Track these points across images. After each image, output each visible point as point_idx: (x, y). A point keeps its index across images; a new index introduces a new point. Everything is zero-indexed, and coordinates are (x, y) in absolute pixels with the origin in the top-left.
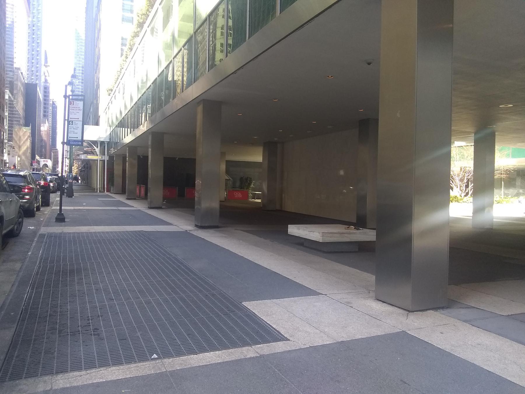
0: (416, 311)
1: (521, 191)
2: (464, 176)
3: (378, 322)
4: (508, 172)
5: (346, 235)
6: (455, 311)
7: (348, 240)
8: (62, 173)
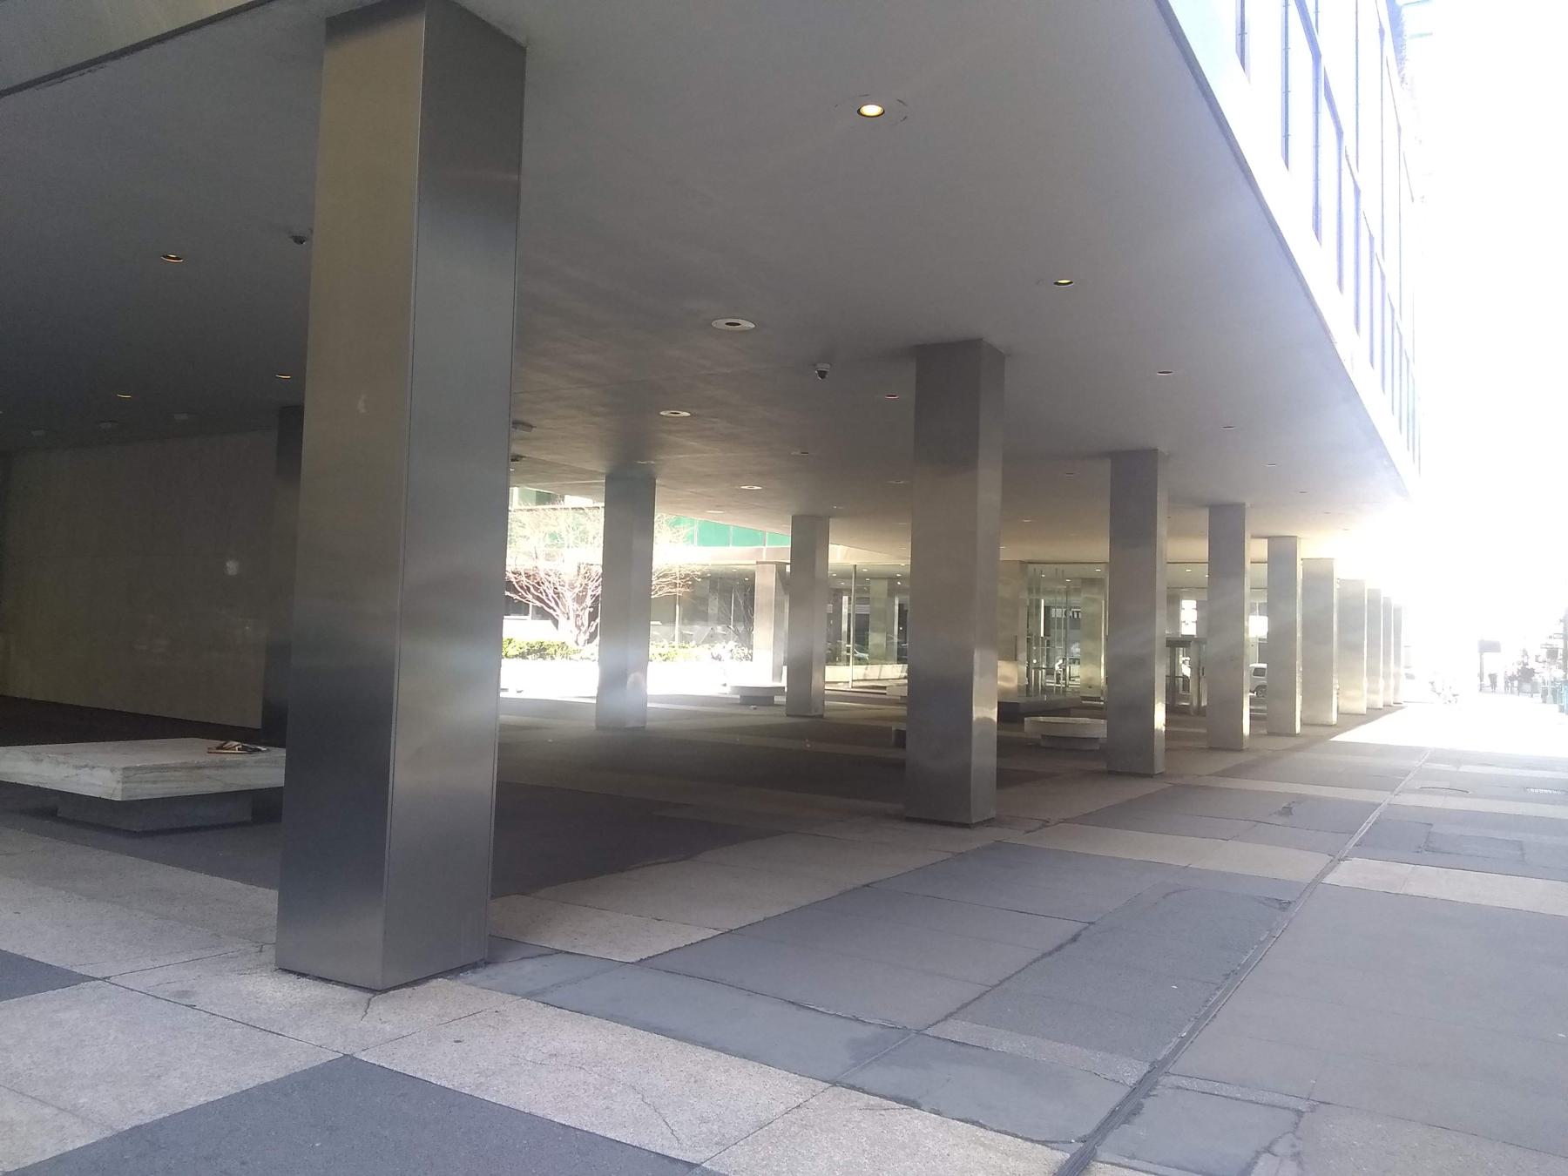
0: (394, 988)
1: (719, 629)
2: (585, 589)
3: (271, 1039)
4: (690, 580)
5: (207, 772)
6: (526, 971)
7: (216, 788)
8: (1199, 702)
